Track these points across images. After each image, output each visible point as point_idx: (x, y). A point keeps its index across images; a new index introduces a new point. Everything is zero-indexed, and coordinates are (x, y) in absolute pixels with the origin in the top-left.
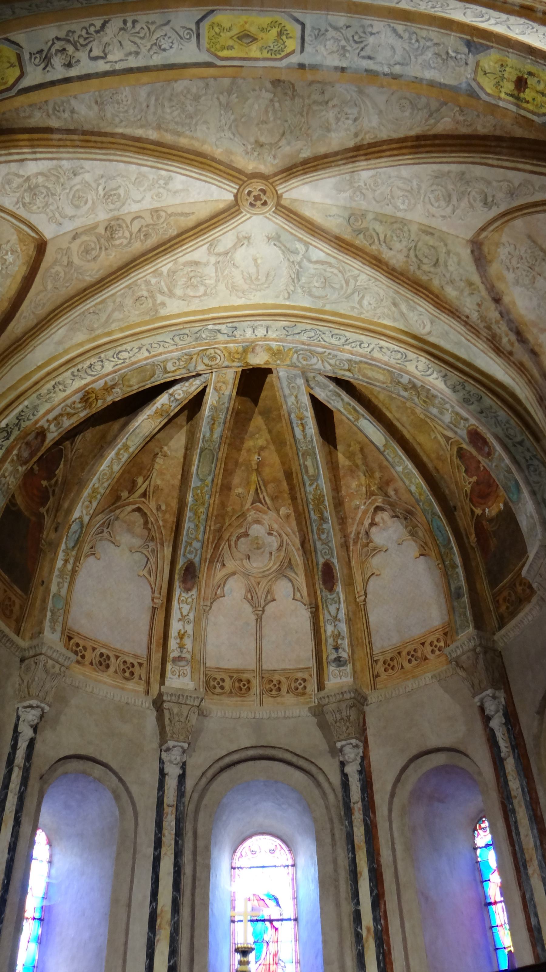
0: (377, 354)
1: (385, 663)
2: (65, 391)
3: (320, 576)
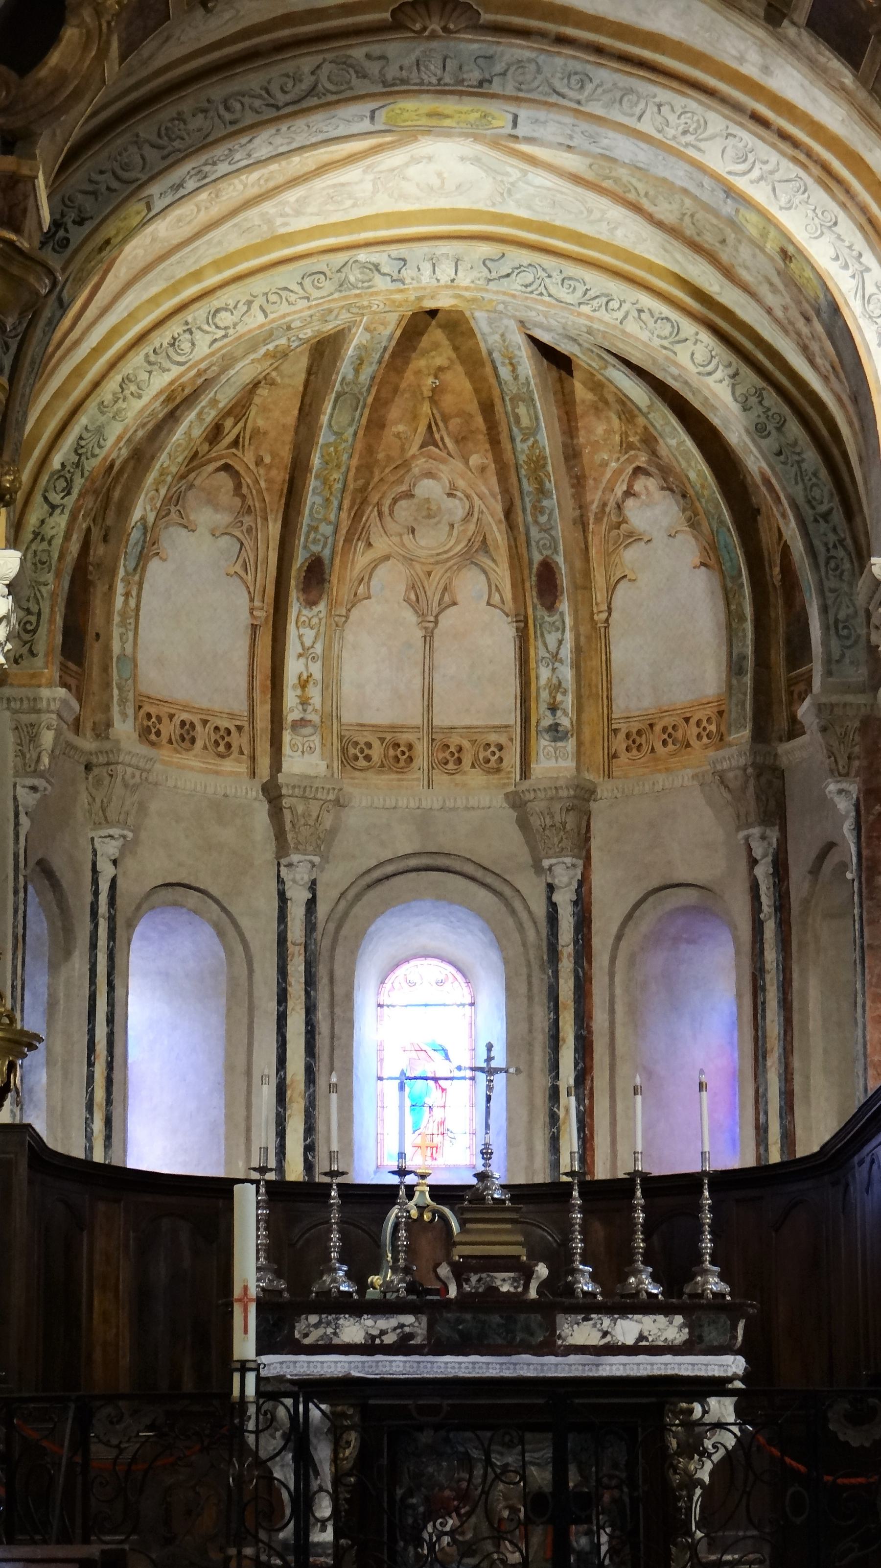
0: (632, 327)
1: (628, 736)
2: (140, 397)
3: (533, 583)
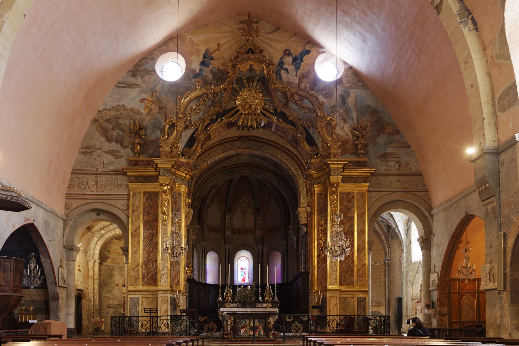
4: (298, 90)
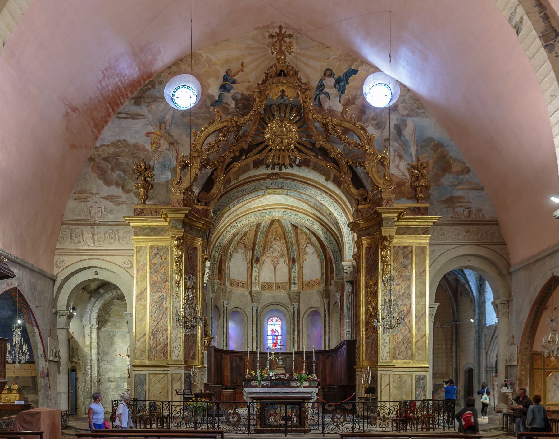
0: (306, 222)
4: (341, 120)
